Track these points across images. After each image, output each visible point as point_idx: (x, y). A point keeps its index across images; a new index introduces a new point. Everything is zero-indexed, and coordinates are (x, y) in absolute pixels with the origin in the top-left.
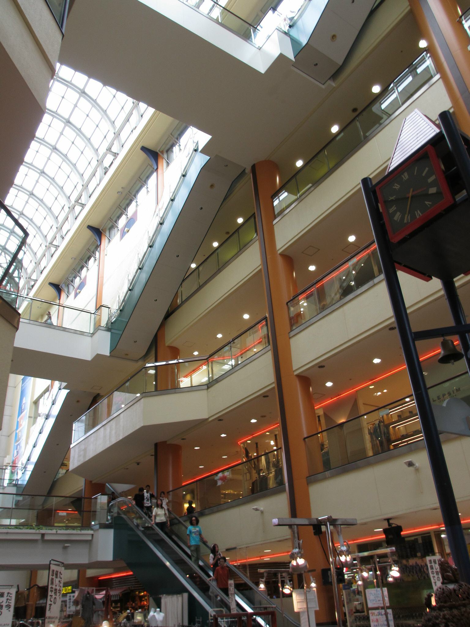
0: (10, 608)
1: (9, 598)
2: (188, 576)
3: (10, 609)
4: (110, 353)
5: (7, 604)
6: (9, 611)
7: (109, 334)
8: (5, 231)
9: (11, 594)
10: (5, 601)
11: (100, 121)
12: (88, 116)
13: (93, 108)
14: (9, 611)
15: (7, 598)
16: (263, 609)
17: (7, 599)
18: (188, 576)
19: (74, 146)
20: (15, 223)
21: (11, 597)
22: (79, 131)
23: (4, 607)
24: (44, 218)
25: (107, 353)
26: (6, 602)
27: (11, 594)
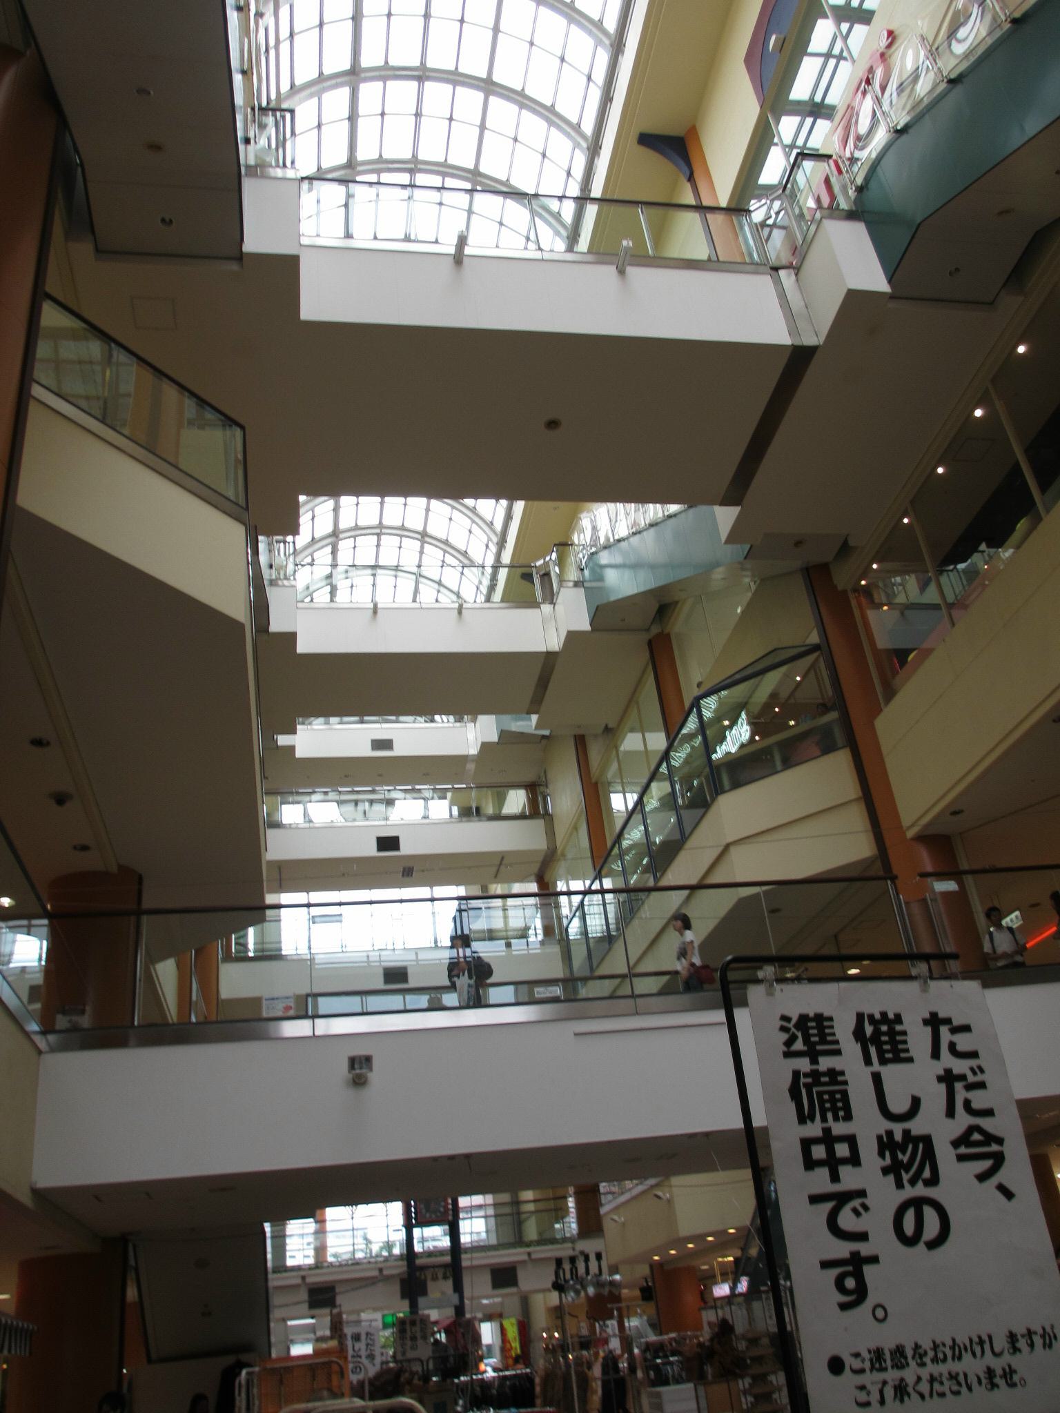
0: (999, 1159)
1: (960, 1066)
2: (5, 1366)
3: (1002, 1176)
4: (591, 625)
5: (963, 1120)
6: (1008, 1194)
7: (581, 591)
8: (436, 546)
9: (966, 1028)
10: (935, 1096)
11: (533, 149)
12: (516, 140)
13: (524, 111)
14: (1008, 1194)
15: (938, 1068)
16: (487, 1278)
17: (948, 1078)
18: (5, 1366)
19: (506, 228)
20: (383, 1202)
21: (974, 1055)
22: (521, 99)
23: (945, 1154)
24: (468, 532)
25: (586, 626)
26: (951, 1113)
27: (966, 1028)
